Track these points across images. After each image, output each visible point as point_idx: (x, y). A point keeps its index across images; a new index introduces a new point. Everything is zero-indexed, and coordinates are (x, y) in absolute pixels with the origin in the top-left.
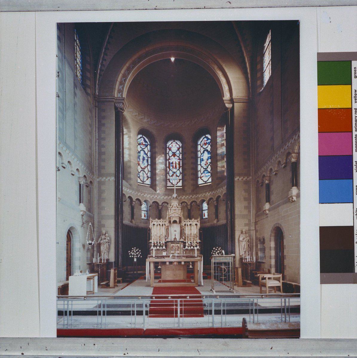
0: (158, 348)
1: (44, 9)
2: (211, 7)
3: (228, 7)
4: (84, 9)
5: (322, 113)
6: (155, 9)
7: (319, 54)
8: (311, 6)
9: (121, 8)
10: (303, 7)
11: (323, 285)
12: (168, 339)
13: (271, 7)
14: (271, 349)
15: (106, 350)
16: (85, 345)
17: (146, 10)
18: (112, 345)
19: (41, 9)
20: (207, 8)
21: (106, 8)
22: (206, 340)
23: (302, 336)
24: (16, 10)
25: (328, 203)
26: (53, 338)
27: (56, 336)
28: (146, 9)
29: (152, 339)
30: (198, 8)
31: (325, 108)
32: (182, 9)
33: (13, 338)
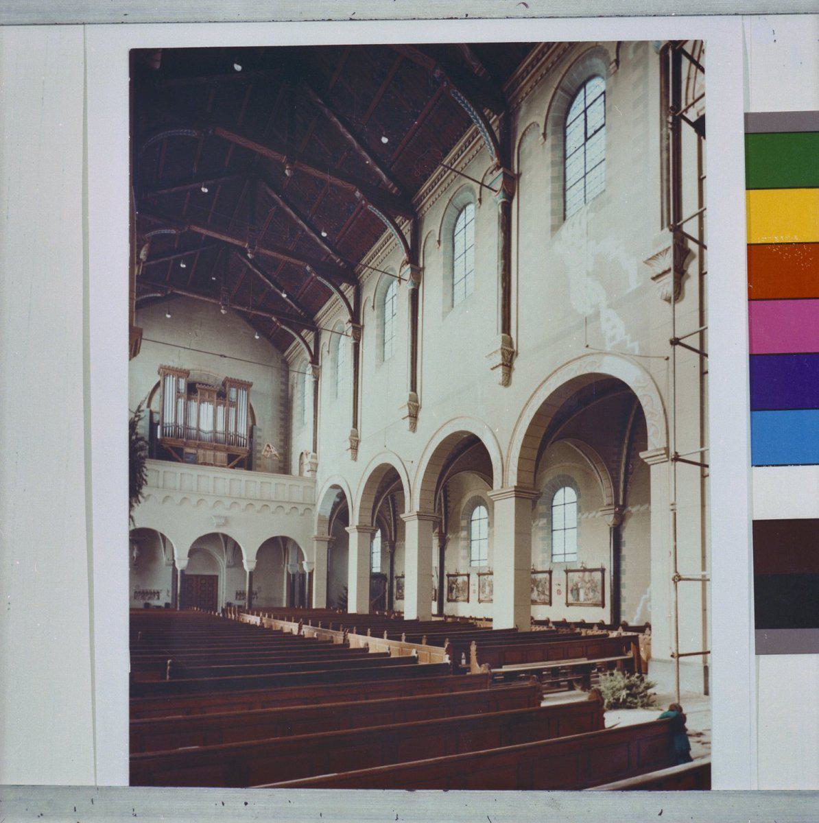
0: (395, 813)
1: (91, 19)
2: (483, 16)
3: (521, 15)
4: (186, 20)
5: (756, 253)
6: (351, 19)
7: (747, 116)
8: (715, 15)
9: (270, 17)
10: (698, 15)
11: (763, 658)
12: (418, 791)
13: (622, 16)
14: (660, 814)
15: (274, 817)
16: (223, 804)
17: (330, 22)
18: (288, 805)
19: (84, 19)
20: (472, 18)
21: (236, 18)
22: (425, 793)
23: (715, 786)
24: (26, 20)
25: (773, 466)
26: (124, 788)
27: (128, 784)
28: (330, 20)
29: (382, 791)
30: (452, 18)
31: (763, 241)
32: (414, 19)
33: (57, 788)
